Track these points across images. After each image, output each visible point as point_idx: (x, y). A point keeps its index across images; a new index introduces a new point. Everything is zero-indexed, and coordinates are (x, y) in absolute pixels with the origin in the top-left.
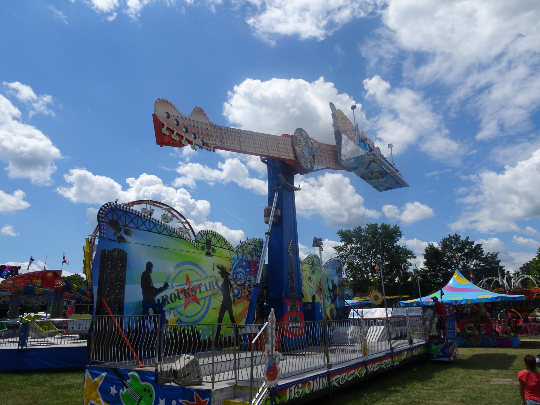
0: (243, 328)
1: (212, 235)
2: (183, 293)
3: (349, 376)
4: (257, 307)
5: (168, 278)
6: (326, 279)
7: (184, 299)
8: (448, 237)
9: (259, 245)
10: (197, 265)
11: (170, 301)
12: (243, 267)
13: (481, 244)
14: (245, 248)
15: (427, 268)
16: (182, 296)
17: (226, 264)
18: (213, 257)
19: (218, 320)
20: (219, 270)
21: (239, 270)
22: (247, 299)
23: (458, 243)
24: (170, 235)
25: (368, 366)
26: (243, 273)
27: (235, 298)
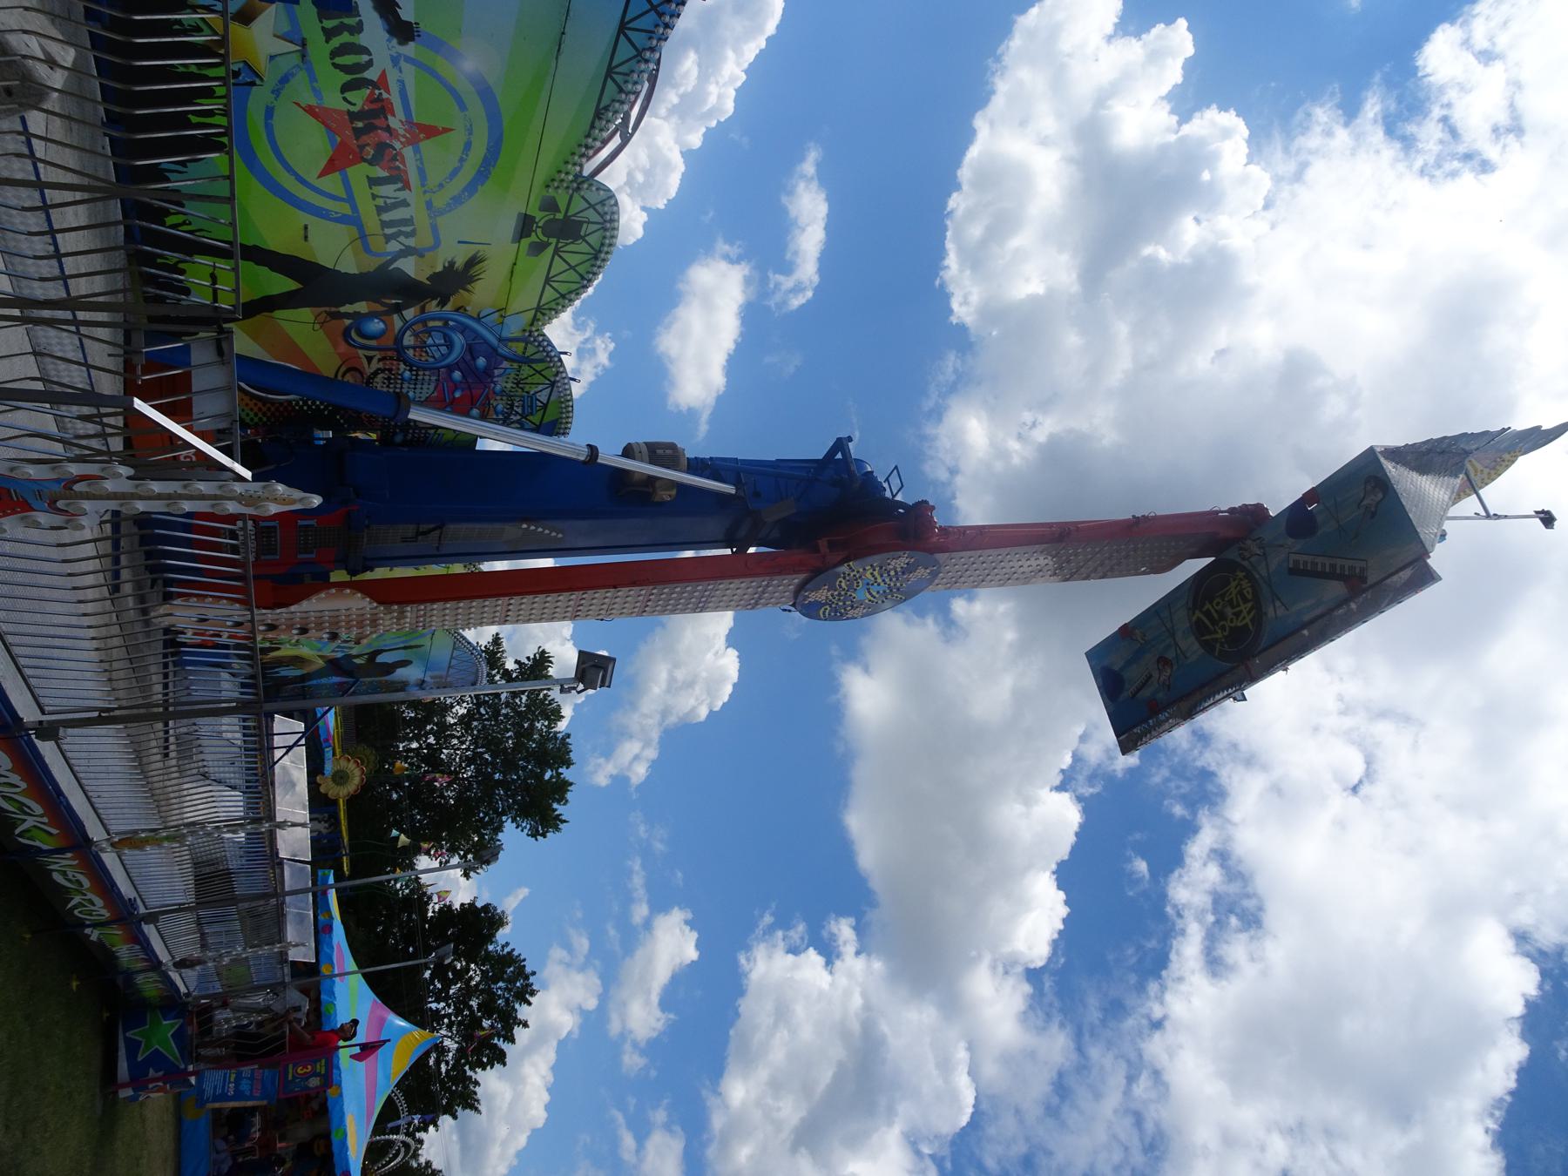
0: (220, 352)
1: (597, 246)
2: (372, 106)
3: (11, 799)
4: (314, 403)
5: (437, 45)
6: (413, 643)
7: (345, 107)
8: (528, 970)
9: (546, 420)
10: (483, 174)
11: (336, 42)
12: (468, 357)
13: (504, 1064)
14: (539, 367)
15: (434, 912)
16: (359, 98)
17: (481, 295)
18: (514, 241)
19: (256, 248)
20: (460, 263)
21: (459, 340)
22: (343, 369)
23: (507, 1000)
24: (610, 72)
25: (69, 855)
26: (444, 357)
27: (348, 322)
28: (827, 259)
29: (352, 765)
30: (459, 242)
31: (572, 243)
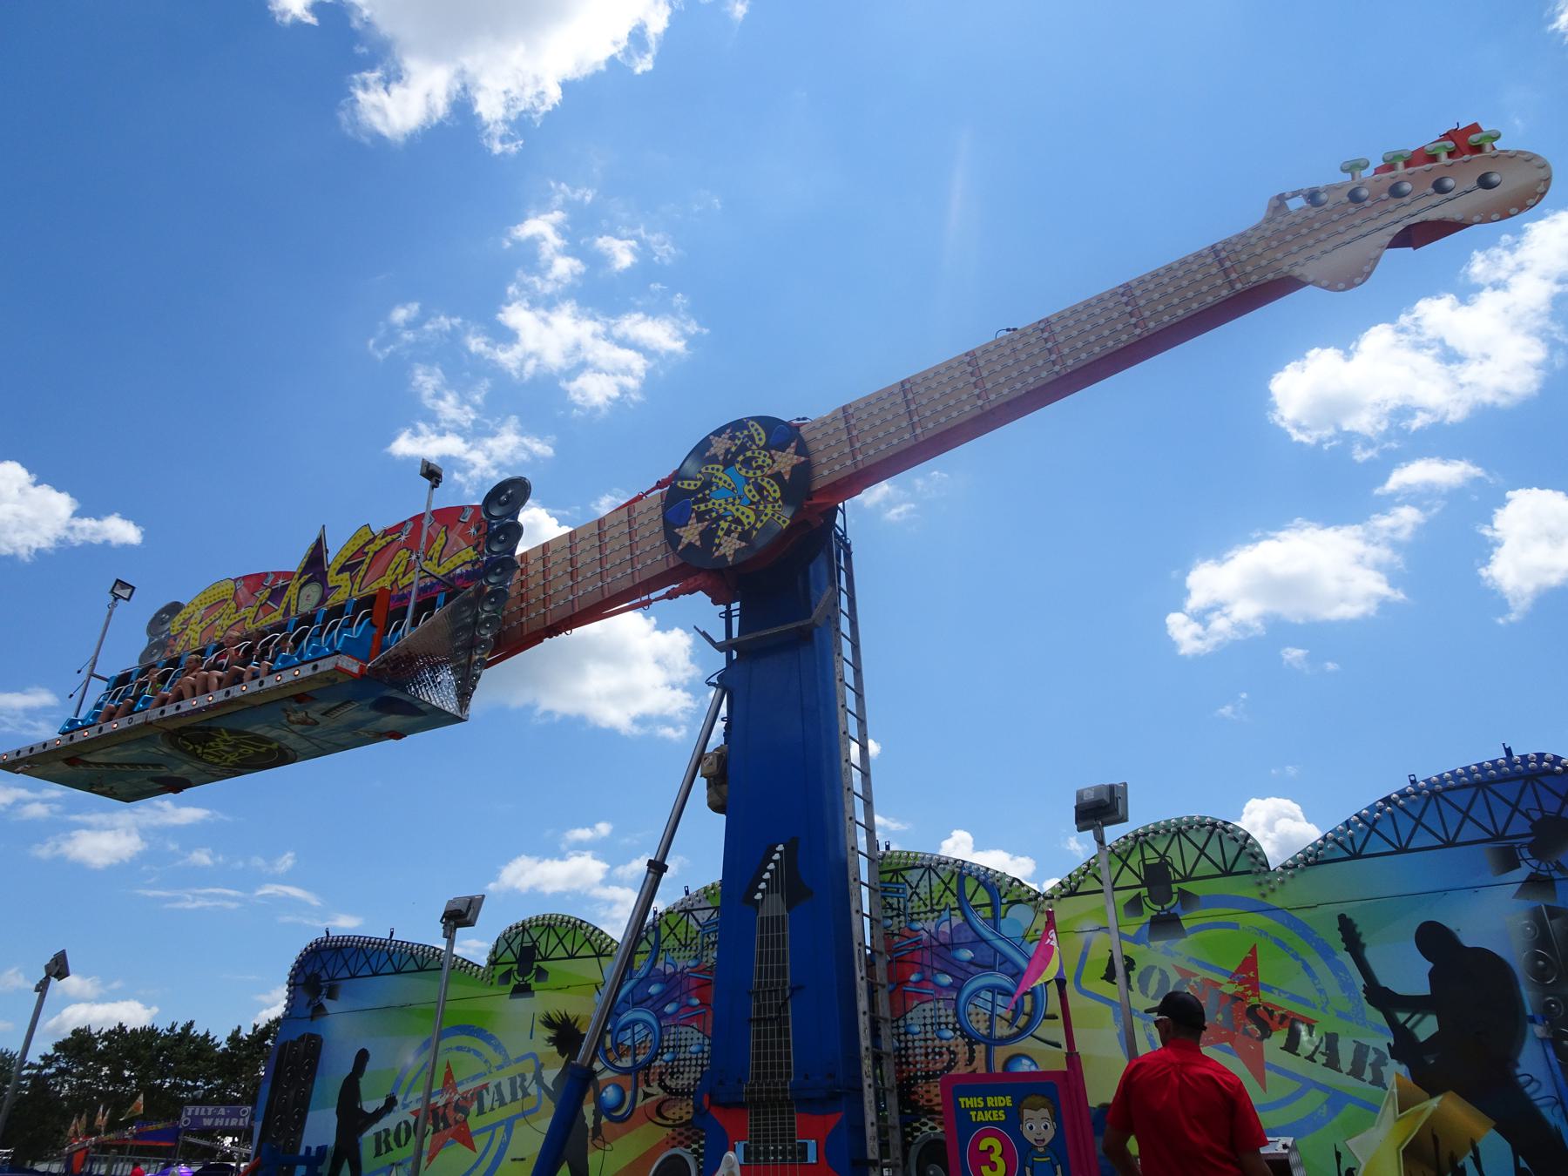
12: (650, 1003)
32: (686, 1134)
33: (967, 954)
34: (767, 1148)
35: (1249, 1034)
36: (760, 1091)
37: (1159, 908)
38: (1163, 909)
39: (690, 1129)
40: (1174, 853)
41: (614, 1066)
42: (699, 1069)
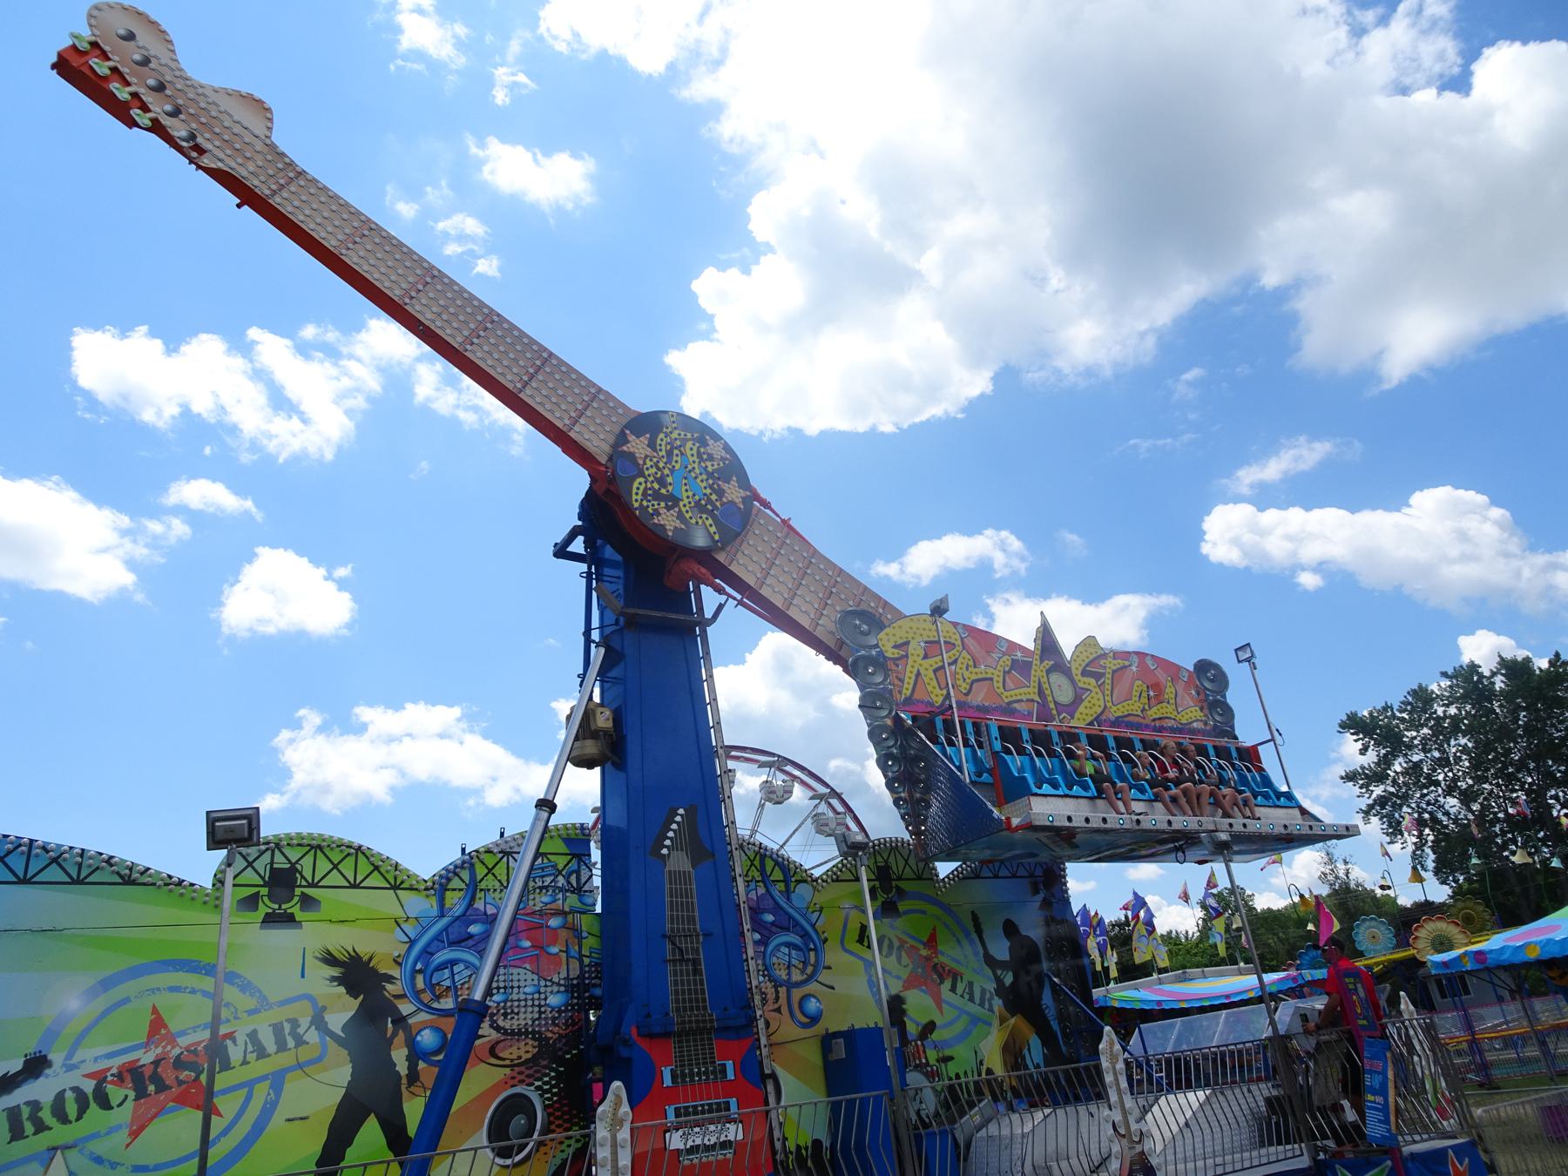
5: (52, 1035)
12: (470, 942)
18: (301, 927)
28: (971, 530)
29: (1422, 933)
30: (303, 976)
31: (301, 873)
32: (527, 1072)
33: (769, 918)
34: (691, 1070)
35: (933, 980)
36: (690, 1022)
37: (276, 906)
38: (280, 908)
39: (531, 1068)
40: (892, 860)
41: (430, 1008)
42: (536, 1009)
